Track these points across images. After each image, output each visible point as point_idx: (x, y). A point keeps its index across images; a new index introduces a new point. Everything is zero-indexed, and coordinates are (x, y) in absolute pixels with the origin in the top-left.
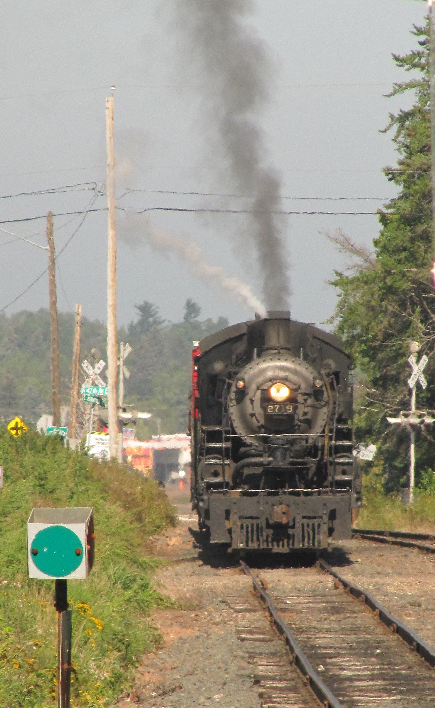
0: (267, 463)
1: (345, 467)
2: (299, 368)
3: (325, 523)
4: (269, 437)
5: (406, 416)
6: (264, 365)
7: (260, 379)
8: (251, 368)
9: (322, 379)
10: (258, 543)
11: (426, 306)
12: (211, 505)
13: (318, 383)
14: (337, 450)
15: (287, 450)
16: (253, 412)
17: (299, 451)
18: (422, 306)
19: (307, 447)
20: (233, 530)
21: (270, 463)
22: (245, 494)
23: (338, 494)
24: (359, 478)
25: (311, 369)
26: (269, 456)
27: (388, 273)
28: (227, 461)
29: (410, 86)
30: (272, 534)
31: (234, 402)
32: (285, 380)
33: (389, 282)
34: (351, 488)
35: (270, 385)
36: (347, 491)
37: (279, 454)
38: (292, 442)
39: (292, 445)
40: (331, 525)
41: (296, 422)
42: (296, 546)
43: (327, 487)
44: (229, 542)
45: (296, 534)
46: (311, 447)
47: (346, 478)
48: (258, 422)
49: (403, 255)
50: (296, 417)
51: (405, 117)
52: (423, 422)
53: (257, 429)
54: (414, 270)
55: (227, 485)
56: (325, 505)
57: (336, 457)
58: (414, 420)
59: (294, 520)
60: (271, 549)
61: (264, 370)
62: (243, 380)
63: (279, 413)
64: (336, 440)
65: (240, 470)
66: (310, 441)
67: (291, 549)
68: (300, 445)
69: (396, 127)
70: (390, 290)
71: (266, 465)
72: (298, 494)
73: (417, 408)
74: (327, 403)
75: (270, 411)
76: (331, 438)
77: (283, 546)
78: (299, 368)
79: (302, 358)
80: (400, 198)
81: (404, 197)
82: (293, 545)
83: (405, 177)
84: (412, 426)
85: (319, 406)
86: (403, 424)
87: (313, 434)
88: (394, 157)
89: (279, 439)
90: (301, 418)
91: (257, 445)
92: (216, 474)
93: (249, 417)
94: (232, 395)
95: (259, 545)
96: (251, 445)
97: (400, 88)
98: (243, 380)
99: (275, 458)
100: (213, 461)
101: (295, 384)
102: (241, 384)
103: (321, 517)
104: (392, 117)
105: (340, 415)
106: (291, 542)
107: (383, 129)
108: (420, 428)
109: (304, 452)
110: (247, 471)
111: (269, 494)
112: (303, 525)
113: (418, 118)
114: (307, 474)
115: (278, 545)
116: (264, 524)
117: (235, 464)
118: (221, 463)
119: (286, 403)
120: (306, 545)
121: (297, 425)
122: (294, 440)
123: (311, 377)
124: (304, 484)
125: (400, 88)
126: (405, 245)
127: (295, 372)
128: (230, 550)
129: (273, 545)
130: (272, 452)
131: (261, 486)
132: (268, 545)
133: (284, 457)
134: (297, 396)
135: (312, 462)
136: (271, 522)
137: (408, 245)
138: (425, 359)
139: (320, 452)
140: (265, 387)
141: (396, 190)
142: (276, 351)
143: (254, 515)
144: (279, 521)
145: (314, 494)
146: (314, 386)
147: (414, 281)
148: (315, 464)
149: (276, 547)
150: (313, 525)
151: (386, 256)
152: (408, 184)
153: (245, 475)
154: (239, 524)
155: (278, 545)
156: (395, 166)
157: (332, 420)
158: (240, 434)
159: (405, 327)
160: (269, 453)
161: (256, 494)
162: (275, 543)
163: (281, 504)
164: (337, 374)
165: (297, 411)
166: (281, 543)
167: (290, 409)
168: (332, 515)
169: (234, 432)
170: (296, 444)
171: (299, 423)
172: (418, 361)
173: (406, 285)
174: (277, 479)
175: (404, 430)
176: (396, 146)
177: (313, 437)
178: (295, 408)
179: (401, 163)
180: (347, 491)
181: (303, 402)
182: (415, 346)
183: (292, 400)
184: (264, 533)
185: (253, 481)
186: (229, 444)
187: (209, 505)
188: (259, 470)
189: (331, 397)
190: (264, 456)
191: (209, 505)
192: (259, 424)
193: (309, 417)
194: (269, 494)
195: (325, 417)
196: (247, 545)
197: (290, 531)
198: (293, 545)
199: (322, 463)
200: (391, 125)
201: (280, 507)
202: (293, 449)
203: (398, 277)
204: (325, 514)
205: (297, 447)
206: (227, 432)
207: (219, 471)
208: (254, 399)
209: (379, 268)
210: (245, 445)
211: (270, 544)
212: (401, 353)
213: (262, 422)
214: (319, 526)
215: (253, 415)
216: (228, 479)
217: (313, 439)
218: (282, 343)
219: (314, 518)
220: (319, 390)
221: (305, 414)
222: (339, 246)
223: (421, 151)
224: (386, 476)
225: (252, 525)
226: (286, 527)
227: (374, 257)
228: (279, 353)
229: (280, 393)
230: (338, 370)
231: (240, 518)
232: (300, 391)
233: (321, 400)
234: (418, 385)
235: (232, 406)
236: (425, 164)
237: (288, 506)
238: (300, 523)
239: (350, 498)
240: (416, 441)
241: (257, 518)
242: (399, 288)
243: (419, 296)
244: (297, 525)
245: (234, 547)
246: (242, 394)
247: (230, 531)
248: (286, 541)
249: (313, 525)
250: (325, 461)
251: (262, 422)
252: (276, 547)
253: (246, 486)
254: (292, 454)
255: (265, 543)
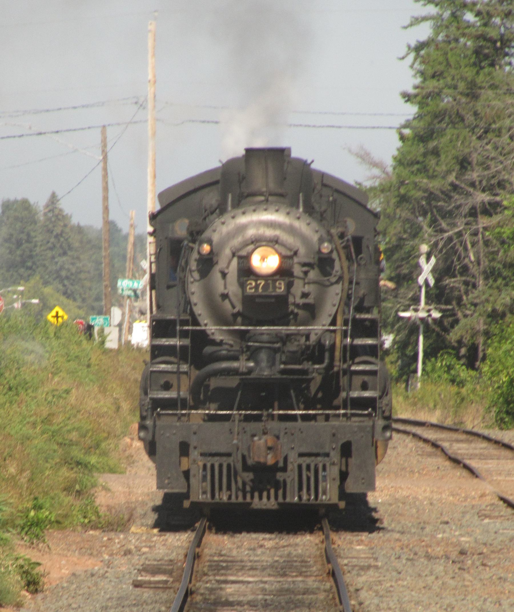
0: (245, 370)
1: (366, 378)
2: (297, 224)
3: (333, 464)
4: (248, 331)
5: (416, 310)
6: (243, 220)
7: (237, 241)
8: (223, 223)
9: (330, 241)
10: (229, 493)
11: (435, 213)
12: (157, 437)
13: (326, 247)
14: (354, 352)
15: (276, 351)
16: (226, 292)
17: (294, 352)
18: (432, 213)
19: (308, 347)
20: (192, 473)
21: (250, 371)
22: (212, 418)
23: (354, 419)
24: (387, 395)
25: (315, 225)
26: (248, 360)
27: (402, 183)
28: (184, 367)
29: (424, 19)
30: (252, 481)
31: (196, 275)
32: (273, 242)
33: (402, 191)
34: (374, 409)
35: (250, 251)
36: (369, 415)
37: (263, 356)
38: (286, 339)
39: (284, 344)
40: (344, 468)
41: (291, 308)
42: (288, 500)
43: (338, 408)
44: (185, 491)
45: (288, 481)
46: (314, 346)
47: (367, 394)
48: (234, 307)
49: (416, 167)
50: (291, 299)
51: (420, 47)
52: (430, 316)
53: (231, 319)
54: (425, 181)
55: (184, 404)
56: (334, 435)
57: (353, 363)
58: (422, 314)
59: (286, 459)
60: (250, 504)
61: (243, 228)
62: (210, 242)
63: (264, 294)
64: (353, 338)
65: (205, 380)
66: (313, 338)
67: (279, 504)
68: (296, 343)
69: (412, 55)
70: (403, 199)
71: (243, 374)
72: (294, 418)
73: (427, 303)
74: (340, 278)
75: (250, 291)
76: (345, 335)
77: (269, 498)
78: (297, 224)
79: (301, 210)
80: (415, 119)
81: (419, 117)
82: (284, 497)
83: (419, 98)
84: (422, 319)
85: (327, 283)
86: (413, 318)
87: (318, 328)
88: (409, 81)
89: (262, 334)
90: (300, 301)
91: (231, 342)
92: (167, 387)
93: (219, 299)
94: (193, 265)
95: (230, 497)
96: (221, 343)
97: (416, 21)
98: (210, 242)
99: (257, 363)
100: (163, 366)
101: (290, 250)
102: (206, 248)
103: (327, 455)
104: (409, 47)
105: (362, 300)
106: (280, 492)
107: (401, 56)
108: (428, 321)
109: (303, 353)
110: (214, 383)
111: (247, 419)
112: (300, 467)
113: (432, 49)
114: (308, 388)
115: (261, 498)
116: (239, 466)
117: (197, 372)
118: (175, 370)
119: (275, 278)
120: (305, 497)
121: (292, 312)
122: (288, 336)
123: (315, 238)
124: (304, 403)
125: (416, 21)
126: (418, 159)
127: (291, 230)
128: (186, 504)
129: (252, 497)
130: (253, 354)
131: (236, 406)
132: (244, 497)
133: (272, 363)
134: (292, 267)
135: (316, 370)
136: (250, 462)
137: (421, 159)
138: (433, 260)
139: (327, 355)
140: (243, 253)
141: (411, 110)
142: (262, 198)
143: (223, 450)
144: (262, 460)
145: (318, 418)
146: (319, 251)
147: (425, 191)
148: (320, 374)
149: (256, 499)
150: (316, 466)
151: (401, 168)
152: (422, 105)
153: (211, 388)
154: (201, 464)
155: (261, 498)
156: (411, 91)
157: (348, 305)
158: (206, 325)
159: (416, 233)
160: (248, 353)
161: (226, 418)
162: (256, 494)
163: (265, 433)
164: (357, 241)
165: (293, 290)
166: (265, 494)
167: (281, 287)
168: (346, 450)
169: (195, 322)
170: (290, 341)
171: (296, 311)
172: (428, 259)
173: (419, 194)
174: (260, 397)
175: (414, 323)
176: (412, 72)
177: (316, 331)
178: (289, 286)
179: (416, 87)
180: (369, 415)
181: (301, 275)
182: (425, 248)
183: (283, 272)
184: (239, 479)
185: (225, 398)
186: (187, 342)
187: (154, 436)
188: (233, 382)
189: (346, 270)
190: (241, 358)
191: (154, 436)
192: (236, 310)
193: (310, 300)
194: (247, 419)
195: (337, 301)
196: (213, 496)
197: (280, 476)
198: (284, 497)
199: (331, 372)
200: (408, 54)
201: (265, 437)
202: (286, 349)
203: (411, 187)
204: (334, 449)
205: (292, 347)
206: (184, 323)
207: (171, 382)
208: (226, 271)
209: (394, 179)
210: (213, 343)
211: (248, 496)
212: (412, 255)
213: (239, 307)
214: (324, 469)
215: (225, 296)
216: (184, 393)
217: (316, 334)
218: (272, 186)
219: (317, 455)
220: (325, 259)
221: (305, 295)
222: (359, 160)
223: (433, 77)
224: (399, 362)
225: (221, 466)
226: (275, 469)
227: (390, 169)
228: (267, 200)
229: (266, 262)
230: (359, 234)
231: (202, 455)
232: (296, 260)
233: (330, 274)
234: (426, 282)
235: (192, 283)
236: (437, 87)
237: (278, 437)
238: (296, 465)
239: (373, 427)
240: (425, 333)
241: (229, 455)
242: (412, 196)
243: (429, 204)
244: (290, 467)
245: (193, 498)
246: (207, 263)
247: (187, 474)
248: (272, 492)
249: (316, 466)
250: (336, 369)
251: (239, 307)
252: (256, 499)
253: (213, 406)
254: (284, 358)
255: (240, 494)
